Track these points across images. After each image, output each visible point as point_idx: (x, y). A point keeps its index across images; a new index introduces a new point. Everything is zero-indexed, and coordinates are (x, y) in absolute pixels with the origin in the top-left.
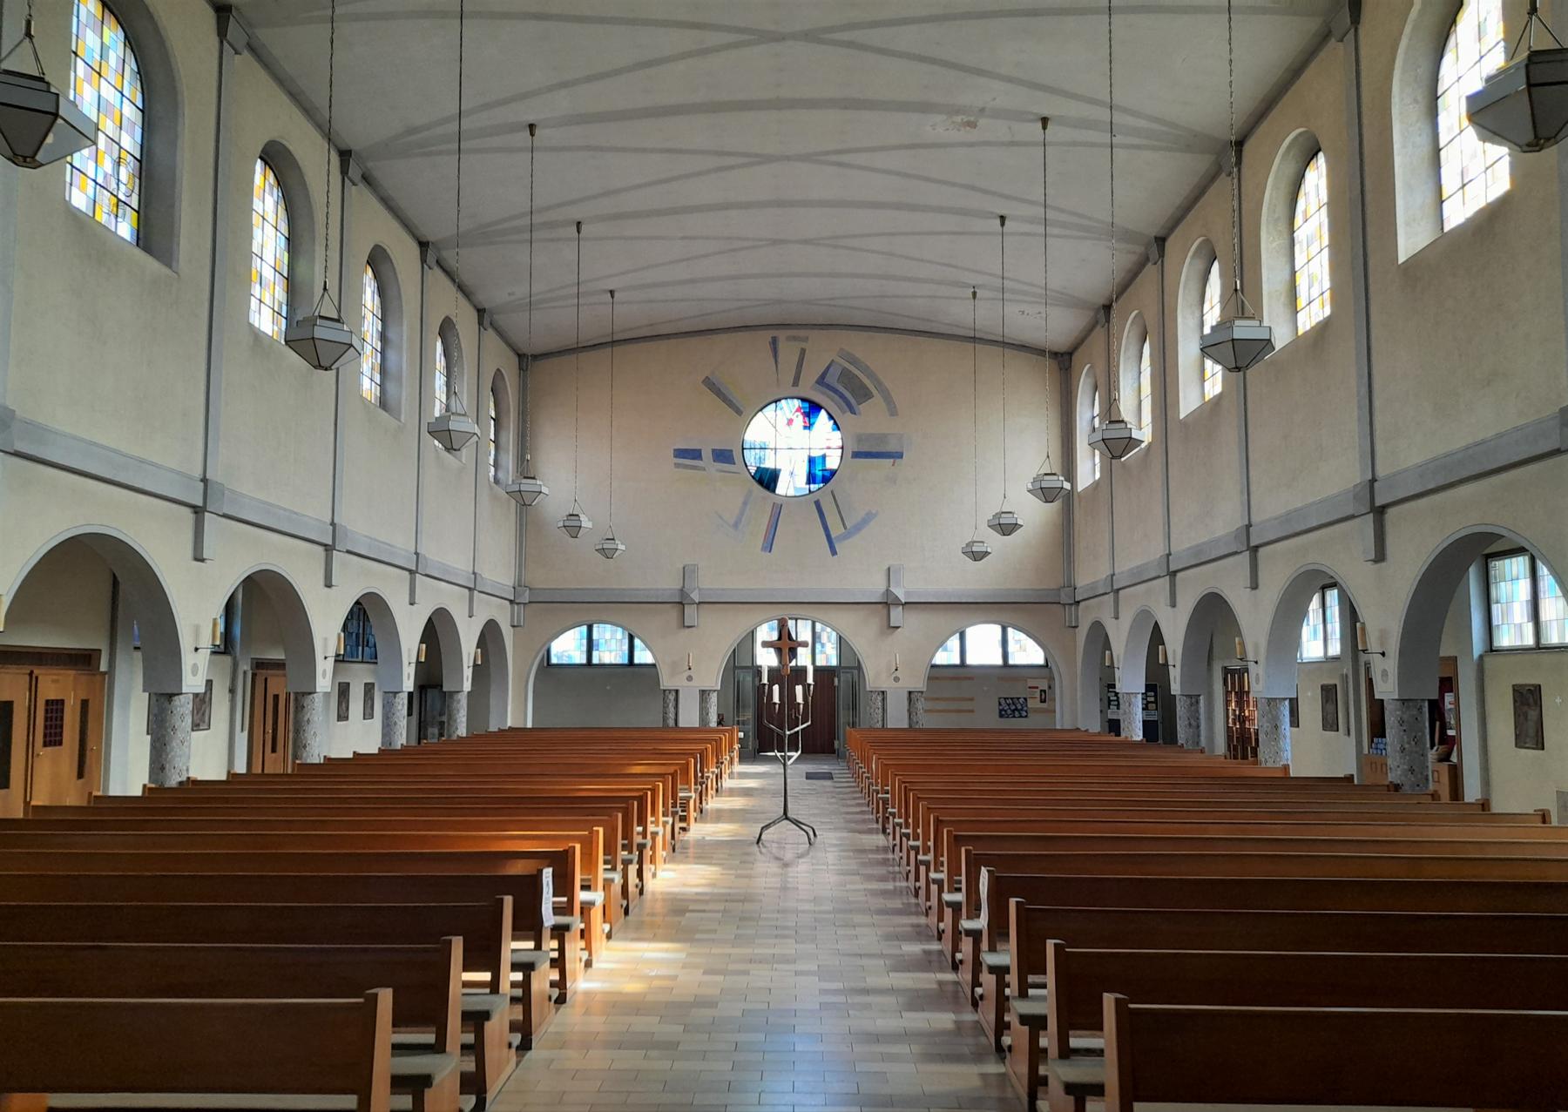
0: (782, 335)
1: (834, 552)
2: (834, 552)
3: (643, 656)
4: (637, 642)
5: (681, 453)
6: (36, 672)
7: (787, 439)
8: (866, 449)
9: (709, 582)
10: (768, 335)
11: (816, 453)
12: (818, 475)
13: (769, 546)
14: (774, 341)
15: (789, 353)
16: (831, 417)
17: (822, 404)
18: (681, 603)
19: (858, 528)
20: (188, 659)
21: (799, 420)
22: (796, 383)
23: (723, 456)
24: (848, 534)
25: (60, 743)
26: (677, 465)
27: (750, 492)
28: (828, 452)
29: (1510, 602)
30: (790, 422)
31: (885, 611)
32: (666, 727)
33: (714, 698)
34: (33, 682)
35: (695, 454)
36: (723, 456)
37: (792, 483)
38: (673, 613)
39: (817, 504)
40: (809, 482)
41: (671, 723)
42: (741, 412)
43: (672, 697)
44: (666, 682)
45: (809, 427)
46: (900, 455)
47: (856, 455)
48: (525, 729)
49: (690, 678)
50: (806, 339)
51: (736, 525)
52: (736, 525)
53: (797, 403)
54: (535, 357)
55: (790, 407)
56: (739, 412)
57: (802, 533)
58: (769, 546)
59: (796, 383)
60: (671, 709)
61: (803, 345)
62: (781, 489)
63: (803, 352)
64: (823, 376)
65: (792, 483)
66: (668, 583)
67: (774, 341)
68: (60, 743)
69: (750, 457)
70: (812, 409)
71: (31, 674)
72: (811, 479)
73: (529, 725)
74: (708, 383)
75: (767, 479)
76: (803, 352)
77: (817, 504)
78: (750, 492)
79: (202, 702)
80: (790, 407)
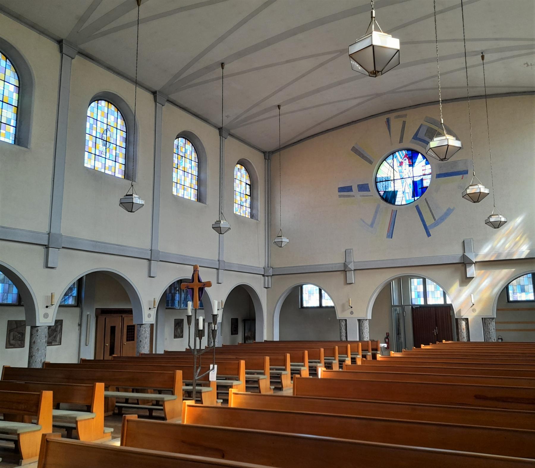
0: (392, 116)
1: (429, 235)
2: (429, 235)
3: (327, 302)
4: (323, 292)
5: (341, 189)
6: (123, 316)
7: (400, 175)
8: (444, 171)
9: (359, 257)
10: (384, 118)
11: (417, 179)
12: (418, 189)
13: (390, 235)
14: (388, 121)
15: (396, 125)
16: (424, 157)
17: (420, 151)
18: (345, 270)
19: (442, 219)
20: (145, 312)
21: (406, 162)
22: (401, 141)
23: (363, 188)
24: (437, 223)
25: (182, 337)
26: (340, 196)
27: (379, 206)
28: (424, 177)
29: (145, 331)
30: (401, 164)
31: (463, 268)
32: (341, 341)
33: (366, 324)
34: (123, 320)
35: (349, 189)
36: (363, 188)
37: (404, 195)
38: (341, 276)
39: (417, 207)
40: (413, 196)
41: (344, 339)
42: (372, 162)
43: (343, 324)
44: (340, 315)
45: (412, 165)
46: (466, 172)
47: (439, 176)
48: (273, 342)
49: (352, 313)
50: (405, 116)
51: (372, 225)
52: (372, 225)
53: (404, 152)
54: (273, 152)
55: (400, 156)
56: (371, 162)
57: (410, 225)
58: (390, 235)
59: (401, 141)
60: (344, 331)
61: (403, 119)
62: (399, 201)
63: (404, 123)
64: (416, 134)
65: (404, 195)
66: (337, 260)
67: (388, 121)
68: (182, 337)
69: (380, 186)
70: (412, 156)
71: (122, 316)
72: (415, 193)
73: (276, 338)
74: (355, 150)
75: (390, 198)
76: (404, 123)
77: (417, 207)
78: (379, 206)
79: (419, 296)
80: (400, 156)
